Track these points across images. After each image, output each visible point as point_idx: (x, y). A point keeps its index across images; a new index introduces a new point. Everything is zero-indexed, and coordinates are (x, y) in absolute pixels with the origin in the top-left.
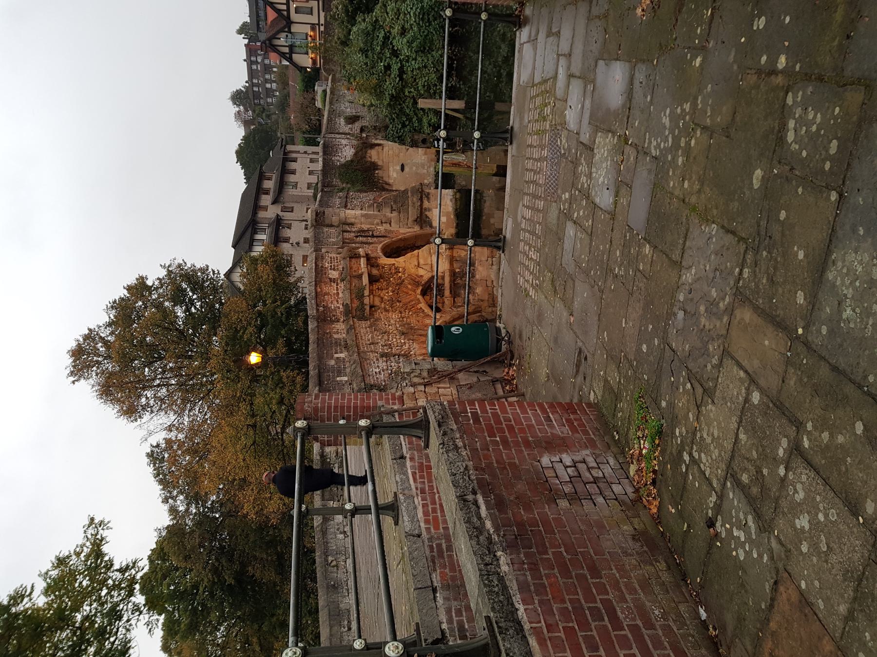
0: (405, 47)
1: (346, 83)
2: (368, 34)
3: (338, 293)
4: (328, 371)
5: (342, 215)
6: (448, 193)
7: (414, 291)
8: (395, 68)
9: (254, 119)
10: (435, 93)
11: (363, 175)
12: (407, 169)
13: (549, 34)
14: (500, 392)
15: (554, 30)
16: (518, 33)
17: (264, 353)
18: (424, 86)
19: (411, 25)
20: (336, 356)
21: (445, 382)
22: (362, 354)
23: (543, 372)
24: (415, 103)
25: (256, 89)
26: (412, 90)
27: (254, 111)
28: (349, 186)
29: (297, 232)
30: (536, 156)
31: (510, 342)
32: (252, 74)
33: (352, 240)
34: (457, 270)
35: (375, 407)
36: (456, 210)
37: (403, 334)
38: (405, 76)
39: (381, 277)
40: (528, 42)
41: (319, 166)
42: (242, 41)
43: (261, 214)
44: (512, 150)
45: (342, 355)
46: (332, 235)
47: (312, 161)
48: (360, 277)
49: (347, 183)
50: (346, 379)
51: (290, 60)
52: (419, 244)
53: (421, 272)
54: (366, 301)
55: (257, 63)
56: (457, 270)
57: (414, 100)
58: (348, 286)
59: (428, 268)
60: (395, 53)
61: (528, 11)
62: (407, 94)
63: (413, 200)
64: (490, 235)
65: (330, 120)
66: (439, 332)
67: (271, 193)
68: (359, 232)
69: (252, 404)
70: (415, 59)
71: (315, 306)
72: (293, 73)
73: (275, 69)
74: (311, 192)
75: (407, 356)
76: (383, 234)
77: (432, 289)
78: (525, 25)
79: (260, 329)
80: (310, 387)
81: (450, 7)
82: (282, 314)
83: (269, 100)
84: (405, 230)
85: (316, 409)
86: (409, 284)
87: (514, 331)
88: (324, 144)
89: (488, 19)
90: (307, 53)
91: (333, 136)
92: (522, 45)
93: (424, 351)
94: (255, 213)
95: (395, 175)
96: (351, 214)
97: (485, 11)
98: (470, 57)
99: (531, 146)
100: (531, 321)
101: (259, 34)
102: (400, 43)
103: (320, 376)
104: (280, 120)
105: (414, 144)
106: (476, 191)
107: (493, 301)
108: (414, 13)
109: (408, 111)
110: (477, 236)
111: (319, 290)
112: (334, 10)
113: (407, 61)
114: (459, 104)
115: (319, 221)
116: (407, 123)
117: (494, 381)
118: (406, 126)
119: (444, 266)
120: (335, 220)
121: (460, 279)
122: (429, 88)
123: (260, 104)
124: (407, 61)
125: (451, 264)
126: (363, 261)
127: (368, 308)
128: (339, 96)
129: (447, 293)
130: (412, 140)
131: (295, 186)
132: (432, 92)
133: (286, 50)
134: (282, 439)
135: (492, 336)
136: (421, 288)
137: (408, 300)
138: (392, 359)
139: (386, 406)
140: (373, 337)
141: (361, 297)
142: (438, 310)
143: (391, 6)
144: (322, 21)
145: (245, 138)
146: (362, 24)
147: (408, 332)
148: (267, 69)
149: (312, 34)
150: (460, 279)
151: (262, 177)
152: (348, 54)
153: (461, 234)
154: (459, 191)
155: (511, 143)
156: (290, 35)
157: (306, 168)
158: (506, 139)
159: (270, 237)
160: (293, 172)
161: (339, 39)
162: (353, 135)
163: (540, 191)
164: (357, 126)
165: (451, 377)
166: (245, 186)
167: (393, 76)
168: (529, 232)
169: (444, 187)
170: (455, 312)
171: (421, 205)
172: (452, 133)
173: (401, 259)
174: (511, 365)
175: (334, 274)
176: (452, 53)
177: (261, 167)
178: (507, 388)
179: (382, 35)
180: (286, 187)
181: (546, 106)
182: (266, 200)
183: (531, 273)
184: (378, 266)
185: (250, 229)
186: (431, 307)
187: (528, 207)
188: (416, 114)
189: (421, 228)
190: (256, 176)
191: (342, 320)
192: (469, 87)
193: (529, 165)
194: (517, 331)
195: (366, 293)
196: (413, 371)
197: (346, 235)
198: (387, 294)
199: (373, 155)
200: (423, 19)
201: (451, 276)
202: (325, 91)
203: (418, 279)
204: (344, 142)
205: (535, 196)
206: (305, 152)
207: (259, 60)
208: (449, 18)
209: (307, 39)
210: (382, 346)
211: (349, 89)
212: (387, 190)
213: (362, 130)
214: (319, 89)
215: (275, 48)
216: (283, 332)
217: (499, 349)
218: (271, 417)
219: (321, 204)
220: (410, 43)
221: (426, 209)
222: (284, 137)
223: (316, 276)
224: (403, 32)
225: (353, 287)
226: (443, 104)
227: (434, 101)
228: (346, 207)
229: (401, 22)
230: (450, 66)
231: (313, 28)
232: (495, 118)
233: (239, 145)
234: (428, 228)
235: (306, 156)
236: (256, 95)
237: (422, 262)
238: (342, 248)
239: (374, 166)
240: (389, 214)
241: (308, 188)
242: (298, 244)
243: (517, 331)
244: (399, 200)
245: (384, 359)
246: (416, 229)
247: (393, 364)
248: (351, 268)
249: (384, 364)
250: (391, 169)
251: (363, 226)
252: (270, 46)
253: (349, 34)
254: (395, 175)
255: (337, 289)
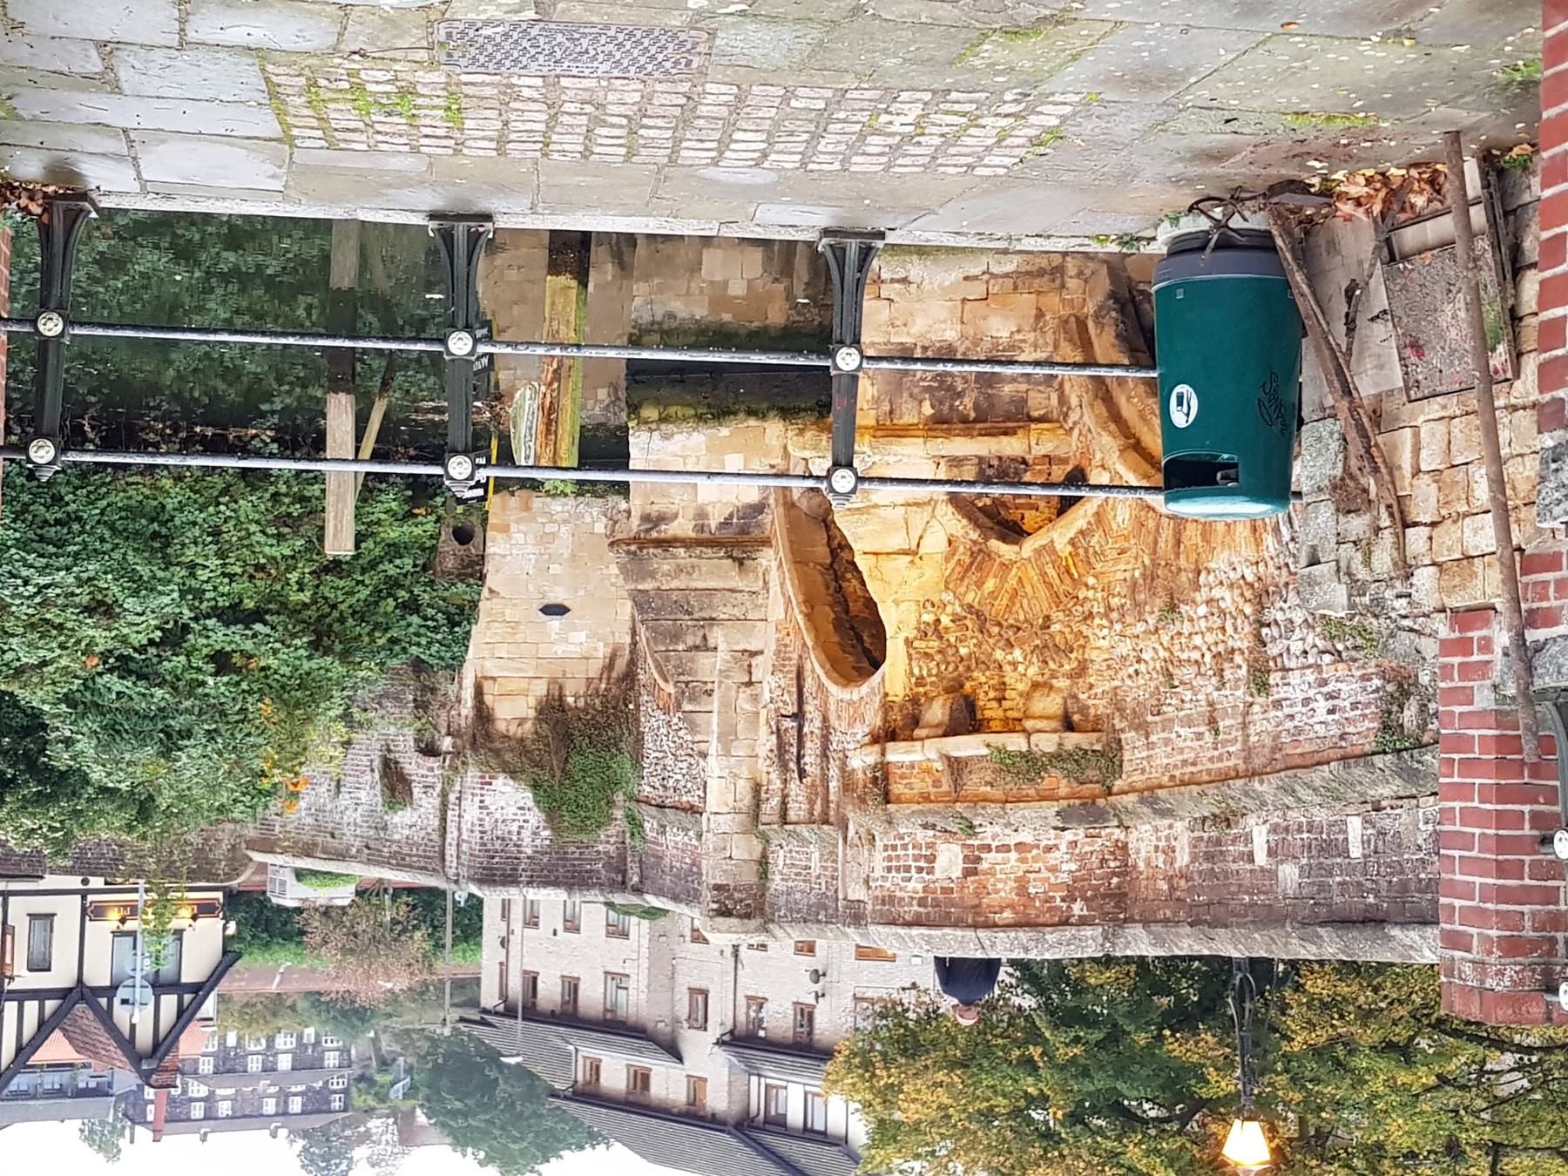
0: (154, 602)
1: (275, 805)
2: (114, 730)
3: (1020, 846)
4: (1323, 887)
5: (726, 823)
6: (643, 446)
7: (1006, 567)
8: (221, 636)
9: (394, 1113)
10: (302, 499)
11: (581, 744)
12: (557, 596)
13: (106, 82)
14: (1435, 230)
15: (95, 65)
16: (105, 203)
17: (1224, 1109)
18: (280, 537)
19: (81, 583)
20: (1261, 859)
21: (1394, 447)
22: (1258, 762)
23: (1376, 58)
24: (336, 566)
25: (296, 1105)
26: (293, 577)
27: (369, 1111)
28: (619, 797)
29: (771, 976)
30: (537, 118)
31: (1235, 198)
32: (246, 1116)
33: (813, 788)
34: (927, 410)
35: (1500, 718)
36: (700, 418)
37: (1172, 608)
38: (249, 604)
39: (955, 687)
40: (137, 166)
41: (551, 900)
42: (140, 1145)
43: (717, 1100)
44: (513, 214)
45: (1260, 838)
46: (798, 862)
47: (532, 921)
48: (956, 767)
49: (611, 803)
50: (1355, 826)
51: (199, 990)
52: (822, 552)
53: (935, 543)
54: (1046, 743)
55: (209, 1100)
56: (927, 410)
57: (326, 570)
58: (993, 809)
59: (919, 518)
60: (173, 637)
61: (28, 167)
62: (305, 597)
63: (667, 574)
64: (790, 296)
65: (399, 861)
66: (1187, 473)
67: (643, 1062)
68: (784, 767)
69: (1412, 1155)
70: (192, 567)
71: (1069, 932)
72: (245, 981)
73: (231, 1040)
74: (639, 928)
75: (1262, 595)
76: (789, 681)
77: (999, 502)
78: (78, 176)
79: (1130, 1120)
80: (1387, 957)
81: (24, 449)
82: (1077, 1040)
83: (331, 1059)
84: (769, 608)
85: (1512, 947)
86: (980, 584)
87: (1190, 182)
88: (481, 882)
89: (60, 309)
90: (179, 933)
91: (451, 851)
92: (145, 188)
93: (1243, 531)
94: (713, 1122)
95: (581, 636)
96: (722, 793)
97: (34, 322)
98: (180, 377)
99: (501, 142)
100: (1159, 115)
101: (118, 1089)
102: (140, 621)
103: (1343, 922)
104: (396, 1024)
105: (473, 570)
106: (635, 342)
107: (1041, 273)
108: (42, 571)
109: (364, 593)
110: (824, 342)
111: (1008, 915)
112: (37, 842)
113: (199, 594)
114: (339, 415)
115: (747, 905)
116: (403, 594)
117: (1392, 255)
118: (415, 599)
119: (914, 457)
120: (744, 849)
121: (966, 399)
122: (285, 519)
123: (346, 1092)
124: (199, 594)
125: (901, 432)
126: (898, 754)
127: (1072, 740)
128: (318, 828)
129: (1011, 446)
130: (462, 577)
131: (617, 979)
132: (301, 511)
133: (169, 1002)
134: (1547, 1050)
135: (1208, 269)
136: (995, 544)
137: (1043, 593)
138: (1273, 650)
139: (1495, 677)
140: (1188, 722)
141: (1032, 765)
142: (1077, 477)
143: (21, 651)
144: (75, 882)
145: (461, 1140)
146: (78, 747)
147: (1165, 589)
148: (229, 1064)
149: (114, 915)
150: (966, 399)
151: (589, 1095)
152: (181, 798)
153: (810, 398)
154: (634, 409)
155: (488, 217)
156: (122, 993)
157: (547, 942)
158: (474, 239)
159: (795, 1070)
160: (572, 987)
161: (130, 828)
162: (448, 782)
163: (667, 96)
164: (415, 766)
165: (1370, 423)
166: (617, 1147)
167: (248, 645)
168: (816, 137)
169: (620, 459)
170: (1085, 415)
171: (687, 543)
172: (457, 436)
173: (889, 615)
174: (1328, 193)
175: (950, 860)
176: (167, 440)
177: (554, 1094)
178: (1419, 201)
179: (115, 683)
180: (621, 1014)
181: (360, 87)
182: (668, 1083)
183: (974, 121)
184: (914, 700)
185: (768, 1139)
186: (1066, 504)
187: (723, 145)
188: (373, 565)
189: (766, 542)
190: (587, 1114)
191: (1118, 834)
192: (280, 382)
193: (569, 142)
194: (1195, 170)
195: (1016, 743)
196: (1343, 571)
197: (796, 810)
198: (1020, 667)
199: (514, 712)
200: (60, 544)
201: (949, 434)
202: (300, 875)
203: (962, 555)
204: (471, 812)
205: (687, 116)
206: (504, 943)
207: (203, 1091)
208: (62, 450)
209: (133, 934)
210: (1222, 685)
211: (295, 795)
212: (632, 662)
213: (430, 751)
214: (291, 894)
215: (163, 1044)
216: (1142, 1039)
217: (1262, 243)
218: (1463, 1087)
219: (689, 896)
220: (139, 587)
221: (701, 528)
222: (455, 1014)
223: (955, 925)
224: (102, 609)
225: (998, 793)
226: (342, 470)
227: (330, 500)
228: (693, 810)
229: (70, 617)
230: (214, 447)
231: (98, 913)
232: (383, 284)
233: (481, 1164)
234: (766, 518)
235: (514, 940)
236: (317, 1103)
237: (897, 541)
238: (844, 826)
239: (552, 709)
240: (721, 658)
241: (624, 935)
242: (817, 976)
243: (1195, 170)
244: (670, 621)
245: (1274, 678)
246: (772, 561)
247: (1297, 647)
248: (926, 798)
249: (1294, 678)
250: (559, 650)
251: (763, 751)
252: (155, 1058)
253: (113, 792)
254: (581, 636)
255: (1005, 848)
